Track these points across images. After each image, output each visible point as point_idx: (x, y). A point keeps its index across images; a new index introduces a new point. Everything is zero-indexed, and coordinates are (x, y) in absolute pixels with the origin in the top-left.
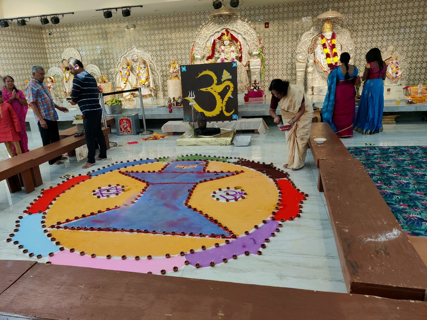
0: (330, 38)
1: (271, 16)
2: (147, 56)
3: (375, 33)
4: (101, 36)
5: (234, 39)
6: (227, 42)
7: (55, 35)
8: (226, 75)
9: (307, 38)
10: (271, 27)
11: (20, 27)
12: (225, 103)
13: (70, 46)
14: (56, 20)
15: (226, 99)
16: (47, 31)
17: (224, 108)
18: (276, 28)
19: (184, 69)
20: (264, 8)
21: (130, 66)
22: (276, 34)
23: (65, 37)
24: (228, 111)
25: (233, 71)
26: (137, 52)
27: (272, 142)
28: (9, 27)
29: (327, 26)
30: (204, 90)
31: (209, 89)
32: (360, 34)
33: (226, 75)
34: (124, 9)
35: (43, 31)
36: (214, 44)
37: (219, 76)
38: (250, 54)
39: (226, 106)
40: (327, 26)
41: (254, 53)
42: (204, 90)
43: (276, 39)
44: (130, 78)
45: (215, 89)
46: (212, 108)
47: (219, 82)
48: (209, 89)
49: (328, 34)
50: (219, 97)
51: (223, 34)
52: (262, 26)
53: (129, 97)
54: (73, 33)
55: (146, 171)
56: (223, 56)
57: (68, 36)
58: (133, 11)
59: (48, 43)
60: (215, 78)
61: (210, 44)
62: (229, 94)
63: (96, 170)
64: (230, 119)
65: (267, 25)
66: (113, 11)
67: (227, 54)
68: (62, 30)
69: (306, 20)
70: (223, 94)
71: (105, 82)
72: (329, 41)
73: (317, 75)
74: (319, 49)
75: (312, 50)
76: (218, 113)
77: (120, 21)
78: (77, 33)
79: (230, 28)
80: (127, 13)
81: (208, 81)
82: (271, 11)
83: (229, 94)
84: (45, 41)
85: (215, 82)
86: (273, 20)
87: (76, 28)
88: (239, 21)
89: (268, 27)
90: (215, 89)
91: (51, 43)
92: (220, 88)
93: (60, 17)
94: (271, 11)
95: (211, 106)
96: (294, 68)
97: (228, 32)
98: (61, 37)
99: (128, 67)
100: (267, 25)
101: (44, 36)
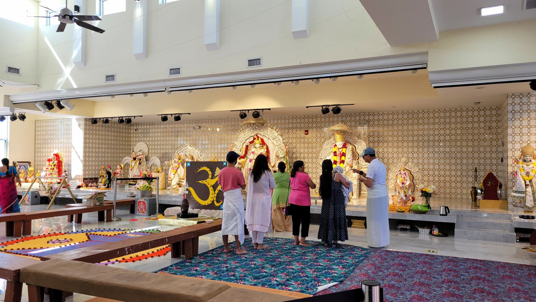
0: (341, 147)
1: (310, 125)
3: (405, 144)
4: (173, 134)
5: (263, 143)
6: (258, 145)
7: (140, 131)
10: (310, 135)
11: (119, 125)
12: (216, 195)
13: (141, 141)
14: (129, 121)
15: (217, 192)
16: (135, 128)
17: (215, 199)
18: (314, 135)
19: (189, 164)
20: (305, 117)
21: (182, 160)
22: (314, 140)
23: (147, 133)
24: (218, 202)
28: (110, 124)
30: (200, 182)
31: (204, 182)
32: (390, 144)
34: (176, 115)
35: (132, 128)
36: (247, 147)
37: (213, 172)
39: (217, 197)
41: (281, 156)
42: (200, 182)
43: (314, 145)
44: (179, 170)
46: (205, 198)
48: (204, 182)
50: (212, 188)
51: (254, 139)
53: (175, 187)
54: (154, 130)
55: (109, 235)
57: (149, 133)
58: (182, 117)
59: (133, 137)
60: (210, 173)
63: (151, 253)
65: (307, 132)
66: (168, 116)
68: (145, 127)
70: (215, 187)
71: (158, 172)
72: (341, 150)
76: (210, 203)
77: (172, 123)
78: (156, 130)
79: (262, 133)
80: (178, 118)
81: (205, 175)
82: (311, 120)
84: (132, 135)
85: (210, 176)
86: (312, 128)
87: (156, 127)
88: (269, 129)
89: (307, 134)
90: (210, 182)
91: (136, 137)
92: (213, 182)
93: (132, 118)
94: (311, 120)
95: (205, 196)
97: (258, 137)
98: (144, 133)
99: (180, 161)
100: (307, 132)
101: (132, 131)
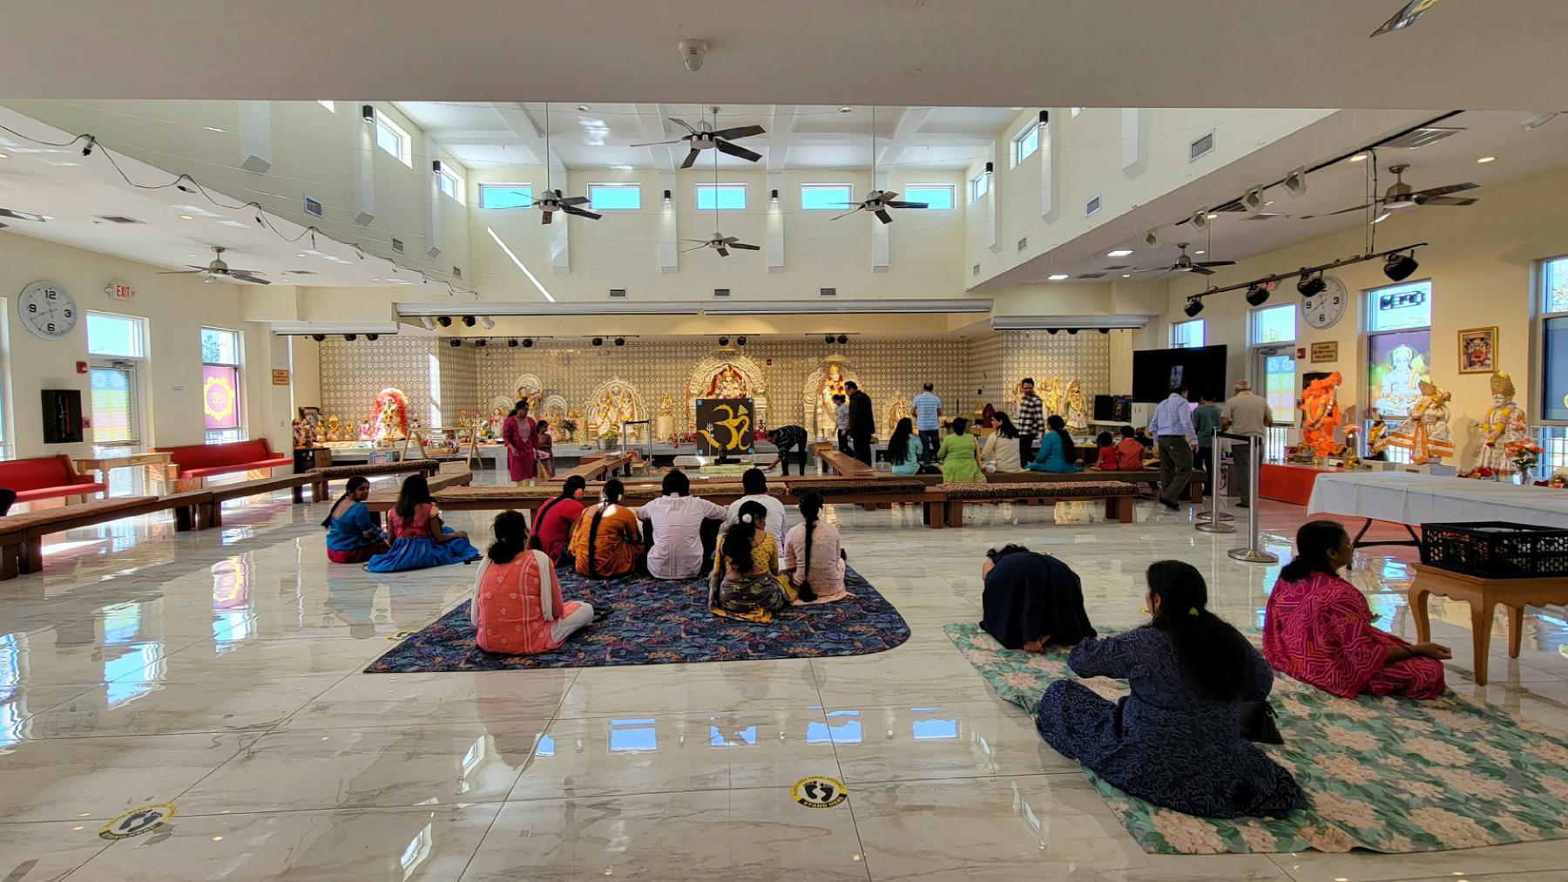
2: (633, 389)
8: (742, 410)
9: (813, 380)
14: (528, 343)
25: (749, 405)
26: (618, 383)
27: (188, 571)
29: (834, 369)
31: (725, 423)
33: (742, 410)
38: (755, 392)
40: (834, 369)
45: (731, 423)
47: (736, 417)
48: (725, 423)
49: (836, 377)
52: (764, 362)
56: (725, 392)
60: (731, 412)
61: (709, 380)
62: (745, 428)
64: (746, 452)
67: (731, 390)
69: (813, 361)
70: (738, 428)
73: (826, 417)
74: (827, 391)
75: (820, 391)
80: (620, 342)
81: (725, 415)
83: (745, 428)
92: (736, 422)
96: (801, 410)
